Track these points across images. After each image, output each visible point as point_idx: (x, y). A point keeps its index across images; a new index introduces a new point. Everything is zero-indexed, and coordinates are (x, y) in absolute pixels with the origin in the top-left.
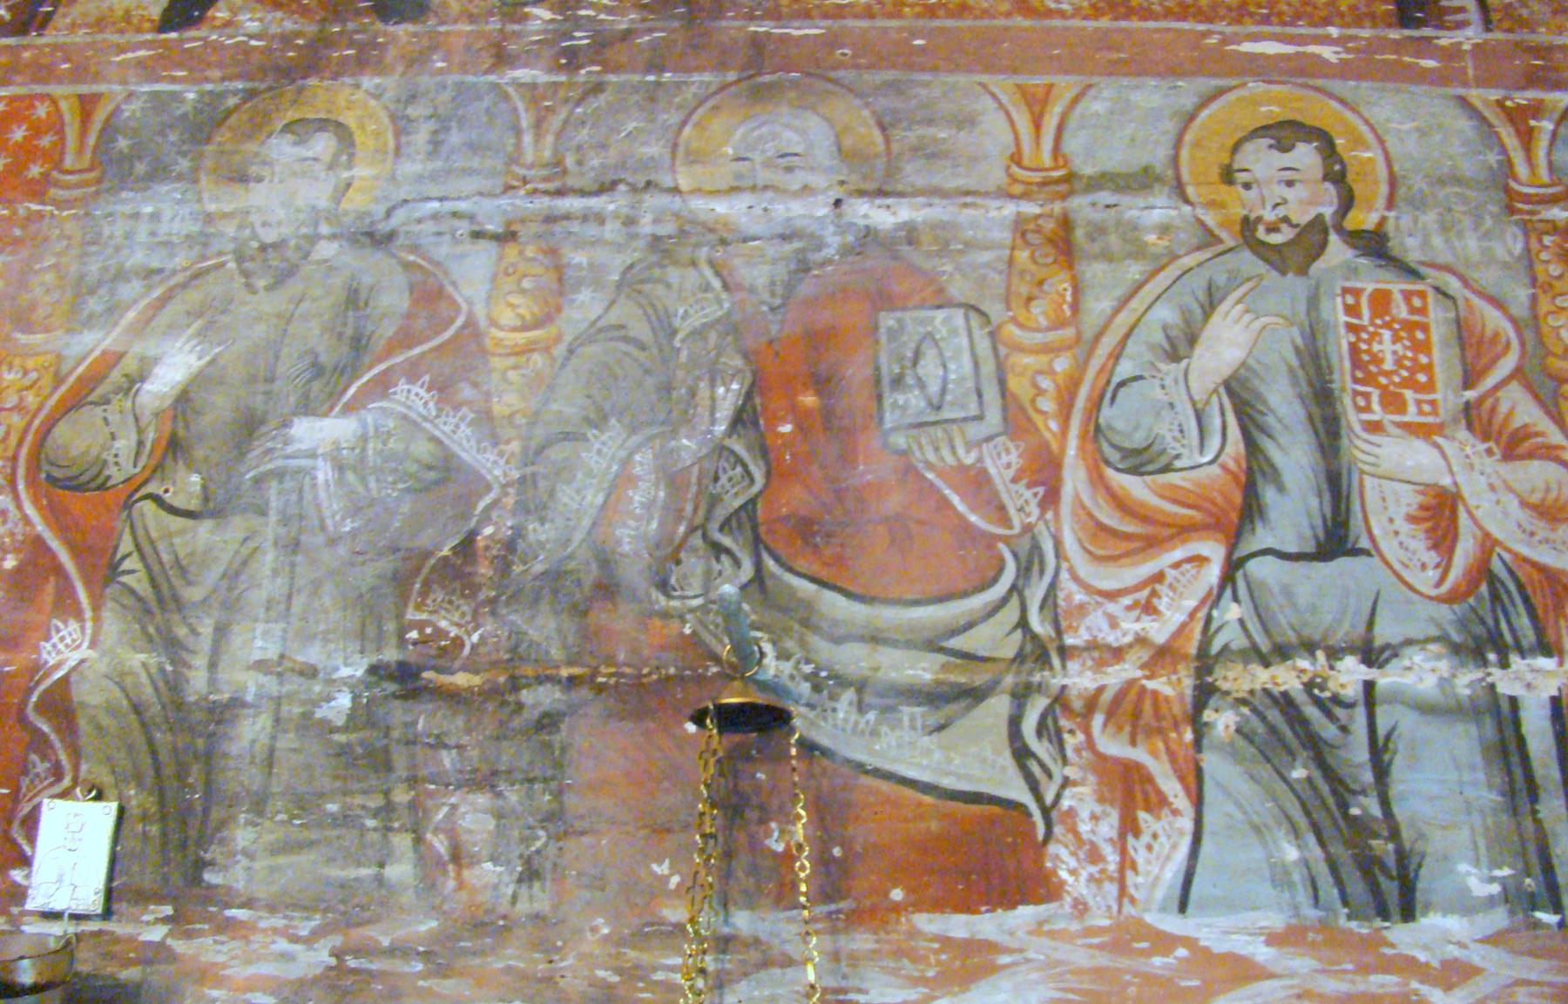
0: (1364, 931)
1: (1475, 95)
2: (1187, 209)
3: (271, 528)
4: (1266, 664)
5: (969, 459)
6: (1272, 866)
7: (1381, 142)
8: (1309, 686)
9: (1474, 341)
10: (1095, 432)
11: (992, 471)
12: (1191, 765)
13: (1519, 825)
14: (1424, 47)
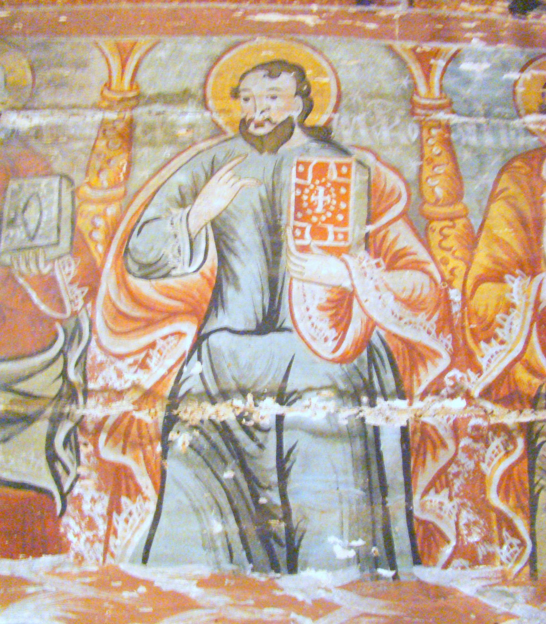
0: (263, 579)
1: (398, 45)
2: (207, 114)
4: (213, 402)
5: (45, 270)
6: (203, 535)
7: (335, 72)
8: (239, 418)
9: (378, 194)
11: (59, 277)
12: (159, 468)
13: (373, 511)
14: (371, 16)
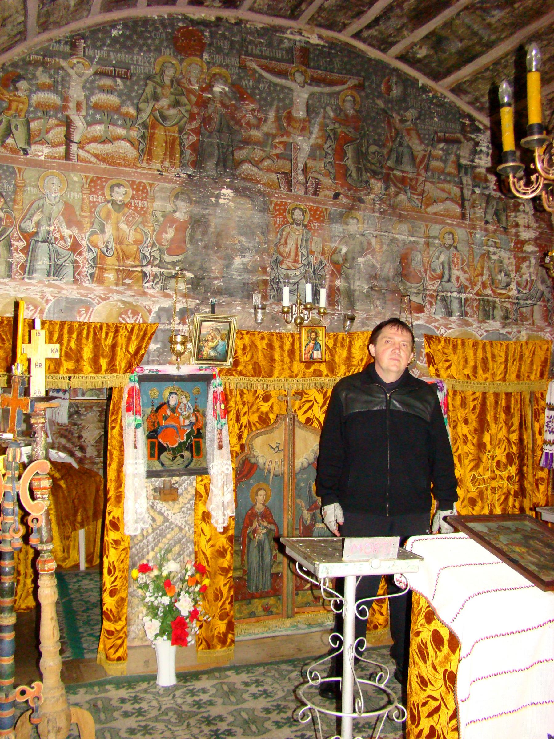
3: (357, 271)
10: (430, 267)
14: (463, 223)
